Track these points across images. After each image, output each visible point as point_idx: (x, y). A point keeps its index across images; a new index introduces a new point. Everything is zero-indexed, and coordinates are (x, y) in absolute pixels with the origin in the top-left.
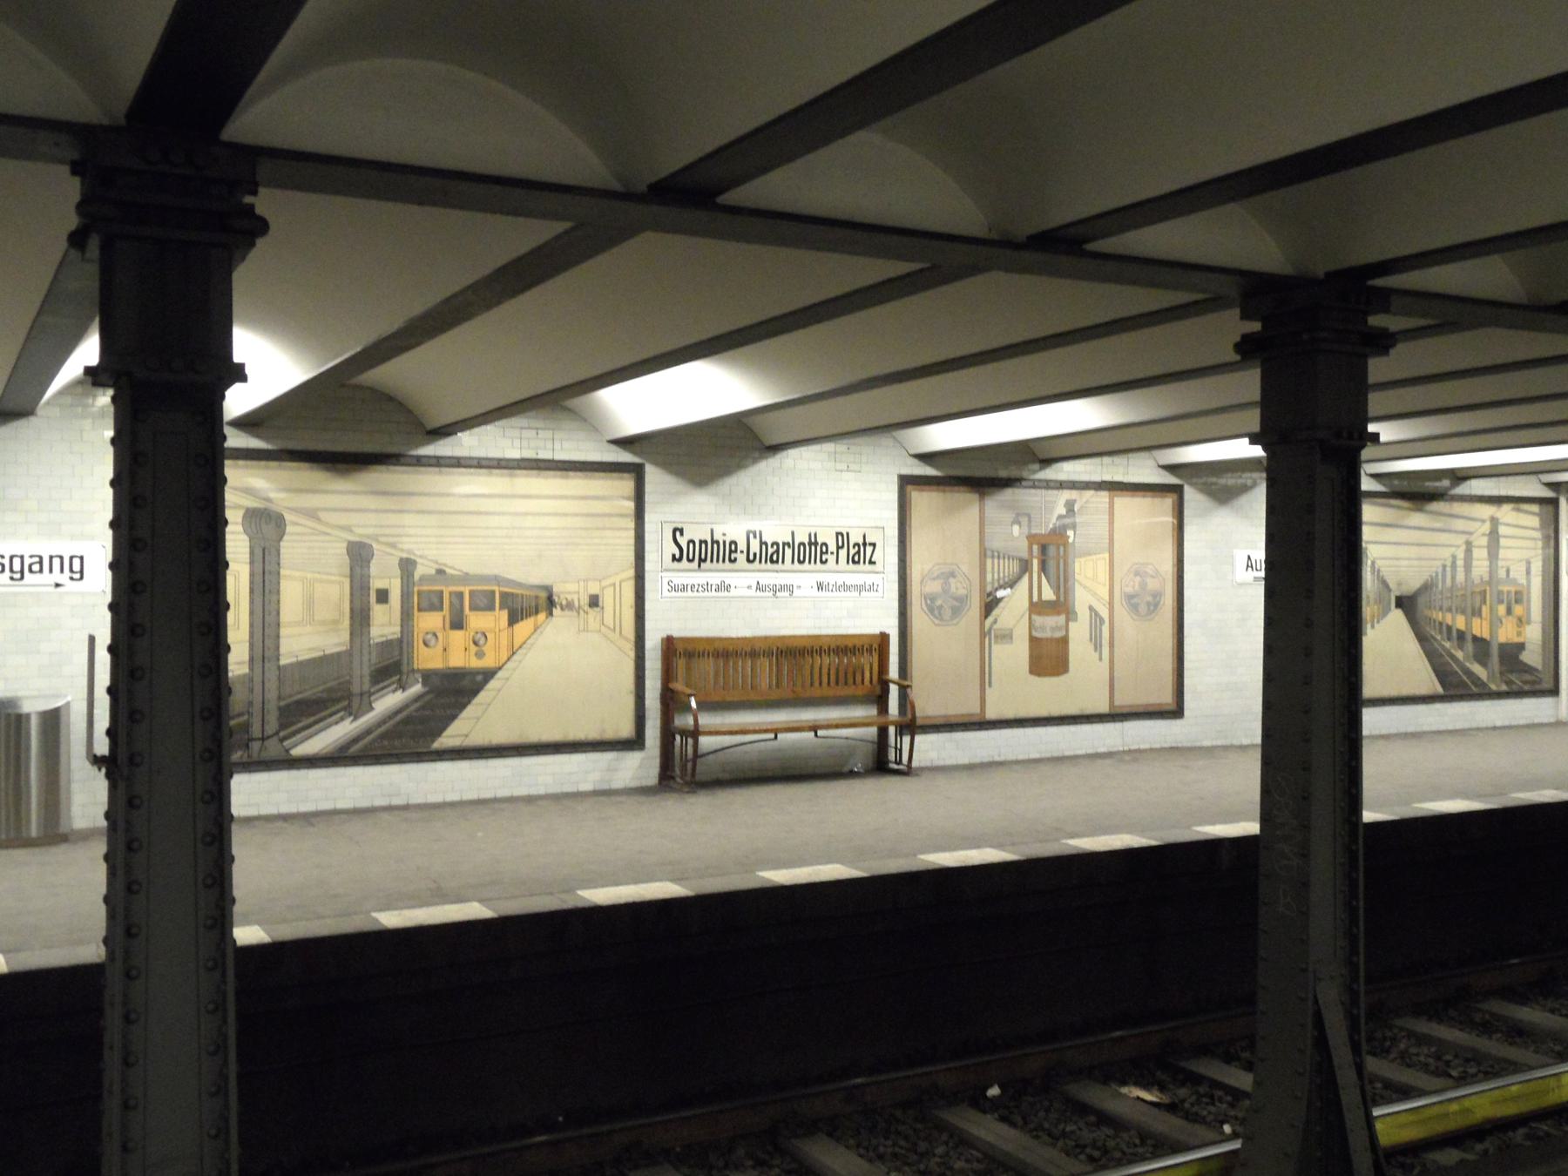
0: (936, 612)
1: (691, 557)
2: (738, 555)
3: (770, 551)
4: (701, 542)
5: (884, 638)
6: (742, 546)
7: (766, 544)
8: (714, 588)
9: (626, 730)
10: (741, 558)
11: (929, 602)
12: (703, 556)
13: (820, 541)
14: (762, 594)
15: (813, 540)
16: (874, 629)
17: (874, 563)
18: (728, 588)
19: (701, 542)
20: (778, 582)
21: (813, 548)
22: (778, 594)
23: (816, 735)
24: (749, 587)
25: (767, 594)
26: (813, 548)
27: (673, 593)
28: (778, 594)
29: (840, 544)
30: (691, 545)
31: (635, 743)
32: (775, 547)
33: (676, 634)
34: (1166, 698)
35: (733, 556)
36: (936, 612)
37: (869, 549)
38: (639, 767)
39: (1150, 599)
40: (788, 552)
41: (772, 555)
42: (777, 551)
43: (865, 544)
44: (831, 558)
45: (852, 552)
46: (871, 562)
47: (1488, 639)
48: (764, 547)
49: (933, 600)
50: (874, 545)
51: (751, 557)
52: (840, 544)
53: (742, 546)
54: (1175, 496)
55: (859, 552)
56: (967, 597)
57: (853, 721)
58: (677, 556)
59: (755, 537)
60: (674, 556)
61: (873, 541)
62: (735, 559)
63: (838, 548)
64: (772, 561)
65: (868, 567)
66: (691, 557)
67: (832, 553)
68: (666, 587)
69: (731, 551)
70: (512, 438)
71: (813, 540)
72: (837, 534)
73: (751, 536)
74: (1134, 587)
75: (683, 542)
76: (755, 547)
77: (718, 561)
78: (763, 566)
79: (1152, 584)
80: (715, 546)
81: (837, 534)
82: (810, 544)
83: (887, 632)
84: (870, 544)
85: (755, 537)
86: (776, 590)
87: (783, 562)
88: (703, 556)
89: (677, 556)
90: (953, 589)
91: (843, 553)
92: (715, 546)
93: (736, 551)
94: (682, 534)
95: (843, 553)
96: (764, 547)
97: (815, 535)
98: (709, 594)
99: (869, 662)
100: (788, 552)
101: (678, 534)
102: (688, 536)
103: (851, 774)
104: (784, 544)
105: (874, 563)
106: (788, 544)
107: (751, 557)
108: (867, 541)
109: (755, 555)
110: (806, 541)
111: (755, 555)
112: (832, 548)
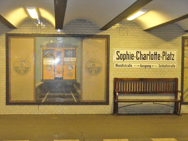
0: (18, 71)
1: (121, 58)
2: (134, 58)
3: (143, 57)
4: (124, 55)
5: (176, 80)
6: (135, 55)
7: (142, 55)
8: (127, 66)
9: (102, 98)
10: (135, 58)
11: (16, 69)
12: (124, 58)
13: (158, 54)
14: (142, 68)
15: (156, 54)
16: (173, 76)
17: (174, 60)
18: (131, 66)
19: (124, 55)
20: (146, 64)
21: (156, 55)
22: (146, 68)
23: (154, 103)
24: (138, 66)
25: (143, 67)
26: (156, 55)
27: (160, 68)
28: (146, 68)
29: (164, 55)
30: (121, 55)
31: (107, 103)
32: (145, 55)
33: (118, 77)
34: (13, 99)
35: (159, 58)
36: (18, 71)
37: (172, 56)
38: (108, 109)
39: (96, 69)
40: (148, 57)
41: (167, 58)
42: (145, 57)
43: (171, 55)
44: (161, 59)
45: (167, 57)
46: (172, 60)
47: (80, 83)
48: (141, 55)
49: (17, 68)
50: (174, 55)
51: (138, 58)
52: (164, 55)
53: (135, 55)
54: (106, 39)
55: (169, 57)
56: (29, 67)
57: (126, 100)
58: (118, 58)
59: (139, 53)
60: (117, 58)
61: (173, 54)
62: (160, 59)
63: (163, 56)
64: (168, 59)
65: (172, 61)
66: (152, 58)
67: (161, 57)
68: (115, 65)
69: (132, 57)
70: (30, 29)
71: (156, 54)
72: (163, 52)
73: (138, 53)
74: (90, 66)
75: (119, 54)
76: (139, 55)
77: (129, 59)
78: (141, 60)
79: (97, 65)
80: (128, 55)
81: (163, 52)
82: (155, 55)
83: (177, 78)
84: (172, 55)
85: (139, 53)
86: (146, 66)
87: (147, 59)
88: (124, 58)
89: (118, 58)
90: (25, 65)
91: (164, 57)
92: (128, 55)
93: (133, 57)
94: (119, 53)
95: (164, 57)
96: (141, 55)
97: (156, 52)
98: (126, 67)
99: (171, 84)
100: (148, 57)
101: (118, 52)
102: (120, 53)
103: (170, 114)
104: (147, 55)
105: (174, 60)
106: (148, 55)
107: (138, 58)
108: (172, 54)
109: (139, 58)
110: (154, 54)
111: (139, 58)
112: (161, 55)
